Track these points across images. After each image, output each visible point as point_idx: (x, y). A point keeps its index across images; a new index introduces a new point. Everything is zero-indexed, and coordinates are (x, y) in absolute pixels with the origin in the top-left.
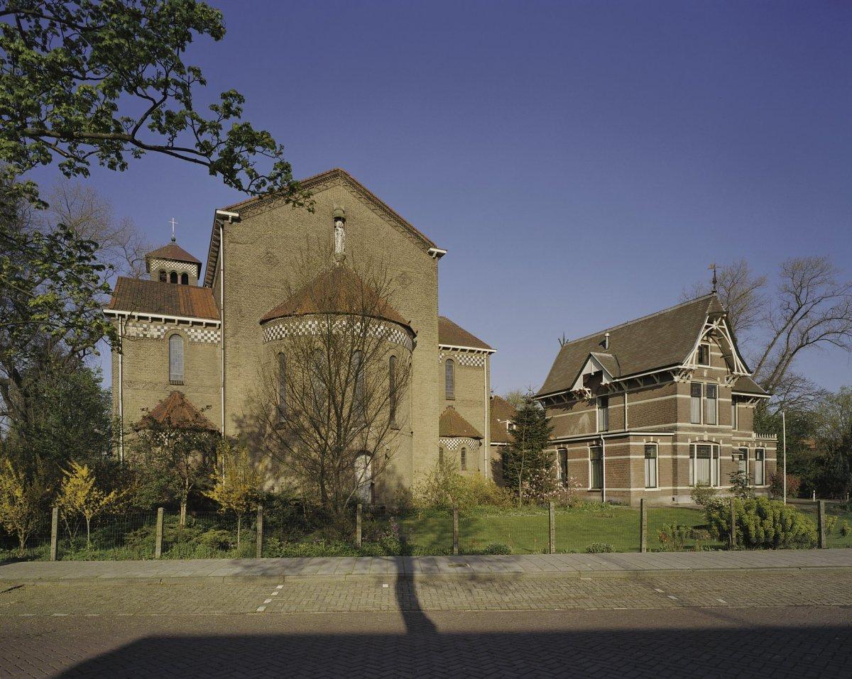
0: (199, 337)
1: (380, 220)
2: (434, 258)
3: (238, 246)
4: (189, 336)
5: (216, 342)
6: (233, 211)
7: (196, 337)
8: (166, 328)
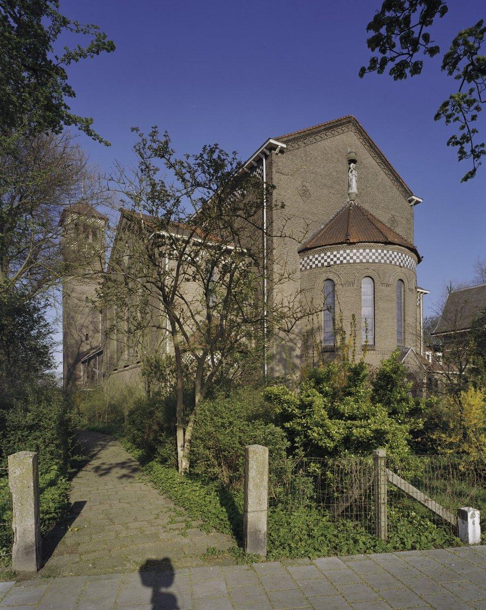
2: (412, 206)
6: (283, 142)
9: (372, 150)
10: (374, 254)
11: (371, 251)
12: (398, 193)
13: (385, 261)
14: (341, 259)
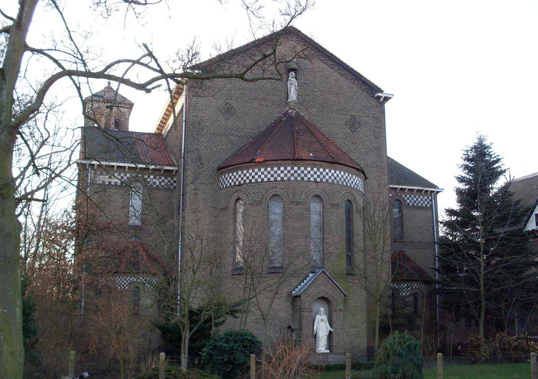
1: (329, 69)
4: (149, 182)
5: (172, 187)
8: (128, 175)
9: (320, 54)
10: (282, 172)
11: (279, 169)
12: (360, 91)
13: (296, 178)
14: (250, 178)
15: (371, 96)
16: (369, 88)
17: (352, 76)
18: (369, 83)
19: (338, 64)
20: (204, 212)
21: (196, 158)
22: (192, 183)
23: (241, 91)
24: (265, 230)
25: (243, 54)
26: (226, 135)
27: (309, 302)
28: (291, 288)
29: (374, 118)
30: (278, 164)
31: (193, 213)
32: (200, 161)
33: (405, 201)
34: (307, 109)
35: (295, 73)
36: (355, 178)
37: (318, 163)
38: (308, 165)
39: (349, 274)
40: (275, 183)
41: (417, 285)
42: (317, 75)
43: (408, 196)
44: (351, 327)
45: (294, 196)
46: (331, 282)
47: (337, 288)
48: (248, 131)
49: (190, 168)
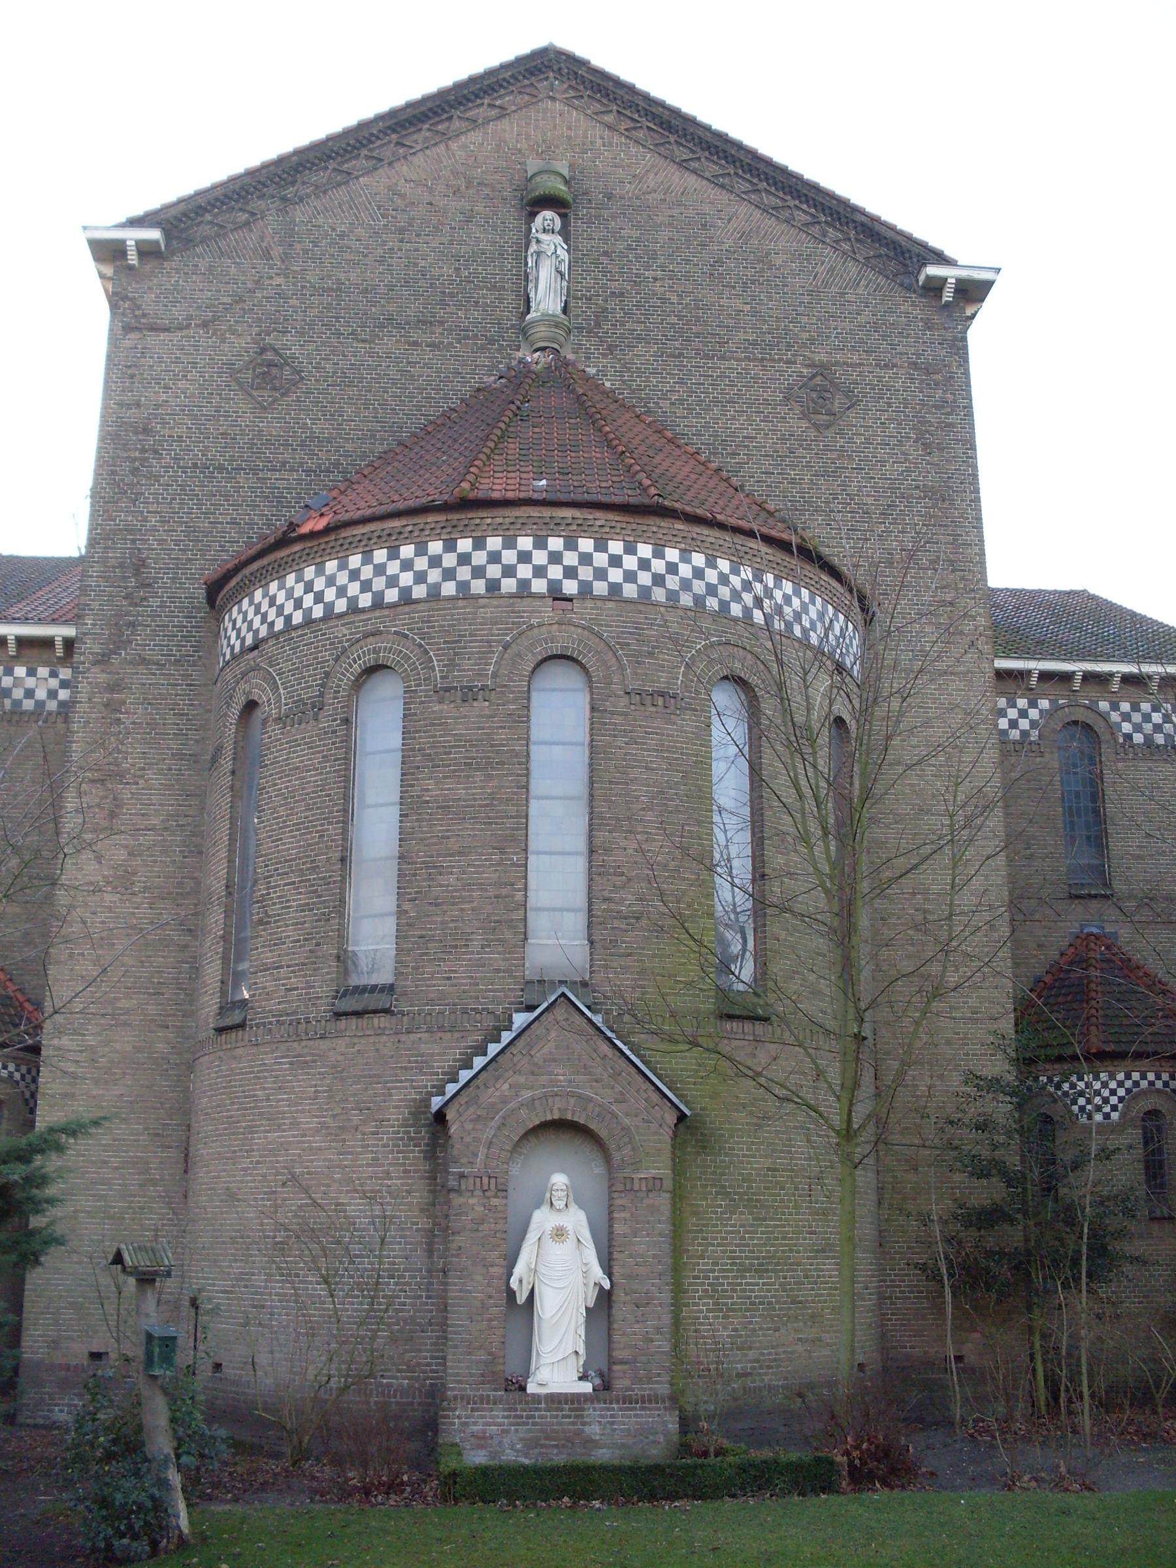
0: (41, 694)
1: (713, 193)
3: (152, 339)
7: (30, 694)
9: (672, 138)
12: (853, 269)
15: (901, 285)
16: (892, 254)
17: (813, 211)
18: (890, 234)
19: (750, 169)
20: (142, 777)
21: (121, 565)
22: (95, 663)
23: (326, 299)
24: (330, 823)
25: (343, 163)
26: (255, 470)
27: (490, 1145)
28: (427, 1081)
29: (916, 369)
30: (390, 535)
31: (97, 781)
32: (137, 573)
33: (1113, 728)
34: (611, 348)
35: (563, 216)
36: (813, 602)
37: (568, 513)
38: (523, 526)
39: (731, 1017)
40: (377, 613)
41: (1158, 1077)
42: (659, 220)
43: (1125, 707)
44: (743, 1270)
45: (451, 665)
46: (605, 1048)
47: (640, 1079)
48: (349, 447)
49: (95, 605)
